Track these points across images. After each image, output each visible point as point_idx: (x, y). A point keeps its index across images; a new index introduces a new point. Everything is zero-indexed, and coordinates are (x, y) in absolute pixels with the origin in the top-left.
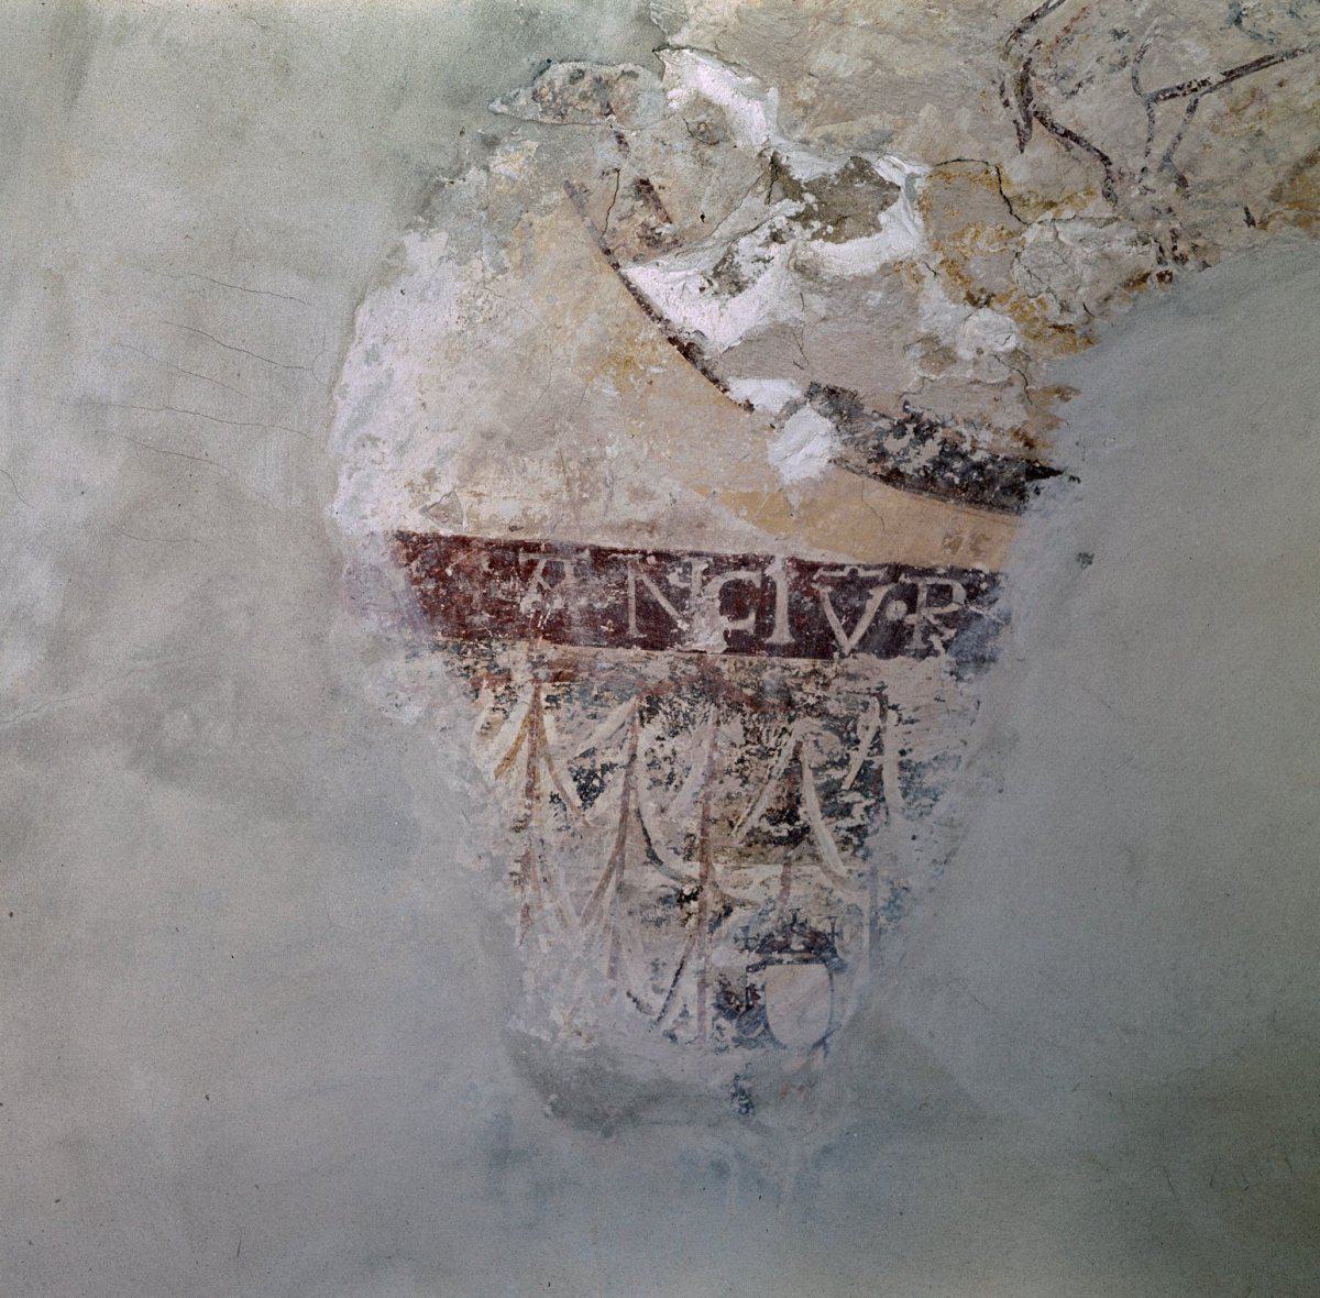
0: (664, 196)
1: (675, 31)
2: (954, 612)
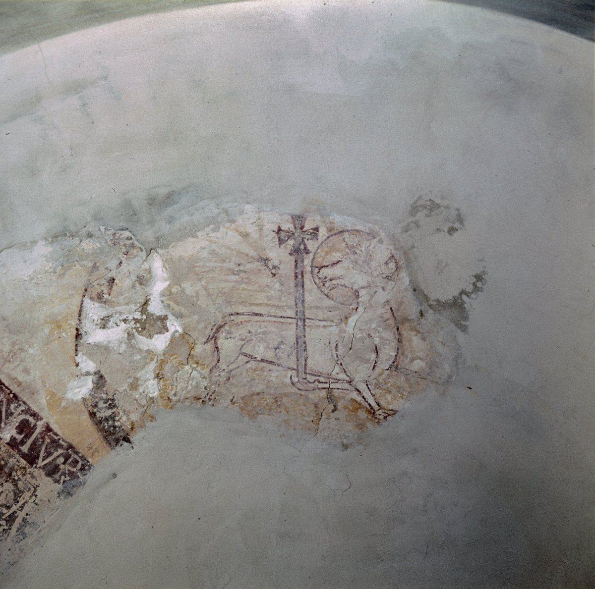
0: (114, 287)
1: (161, 248)
2: (74, 472)
